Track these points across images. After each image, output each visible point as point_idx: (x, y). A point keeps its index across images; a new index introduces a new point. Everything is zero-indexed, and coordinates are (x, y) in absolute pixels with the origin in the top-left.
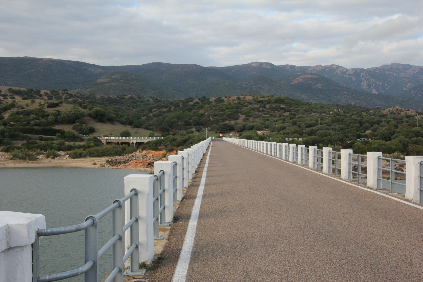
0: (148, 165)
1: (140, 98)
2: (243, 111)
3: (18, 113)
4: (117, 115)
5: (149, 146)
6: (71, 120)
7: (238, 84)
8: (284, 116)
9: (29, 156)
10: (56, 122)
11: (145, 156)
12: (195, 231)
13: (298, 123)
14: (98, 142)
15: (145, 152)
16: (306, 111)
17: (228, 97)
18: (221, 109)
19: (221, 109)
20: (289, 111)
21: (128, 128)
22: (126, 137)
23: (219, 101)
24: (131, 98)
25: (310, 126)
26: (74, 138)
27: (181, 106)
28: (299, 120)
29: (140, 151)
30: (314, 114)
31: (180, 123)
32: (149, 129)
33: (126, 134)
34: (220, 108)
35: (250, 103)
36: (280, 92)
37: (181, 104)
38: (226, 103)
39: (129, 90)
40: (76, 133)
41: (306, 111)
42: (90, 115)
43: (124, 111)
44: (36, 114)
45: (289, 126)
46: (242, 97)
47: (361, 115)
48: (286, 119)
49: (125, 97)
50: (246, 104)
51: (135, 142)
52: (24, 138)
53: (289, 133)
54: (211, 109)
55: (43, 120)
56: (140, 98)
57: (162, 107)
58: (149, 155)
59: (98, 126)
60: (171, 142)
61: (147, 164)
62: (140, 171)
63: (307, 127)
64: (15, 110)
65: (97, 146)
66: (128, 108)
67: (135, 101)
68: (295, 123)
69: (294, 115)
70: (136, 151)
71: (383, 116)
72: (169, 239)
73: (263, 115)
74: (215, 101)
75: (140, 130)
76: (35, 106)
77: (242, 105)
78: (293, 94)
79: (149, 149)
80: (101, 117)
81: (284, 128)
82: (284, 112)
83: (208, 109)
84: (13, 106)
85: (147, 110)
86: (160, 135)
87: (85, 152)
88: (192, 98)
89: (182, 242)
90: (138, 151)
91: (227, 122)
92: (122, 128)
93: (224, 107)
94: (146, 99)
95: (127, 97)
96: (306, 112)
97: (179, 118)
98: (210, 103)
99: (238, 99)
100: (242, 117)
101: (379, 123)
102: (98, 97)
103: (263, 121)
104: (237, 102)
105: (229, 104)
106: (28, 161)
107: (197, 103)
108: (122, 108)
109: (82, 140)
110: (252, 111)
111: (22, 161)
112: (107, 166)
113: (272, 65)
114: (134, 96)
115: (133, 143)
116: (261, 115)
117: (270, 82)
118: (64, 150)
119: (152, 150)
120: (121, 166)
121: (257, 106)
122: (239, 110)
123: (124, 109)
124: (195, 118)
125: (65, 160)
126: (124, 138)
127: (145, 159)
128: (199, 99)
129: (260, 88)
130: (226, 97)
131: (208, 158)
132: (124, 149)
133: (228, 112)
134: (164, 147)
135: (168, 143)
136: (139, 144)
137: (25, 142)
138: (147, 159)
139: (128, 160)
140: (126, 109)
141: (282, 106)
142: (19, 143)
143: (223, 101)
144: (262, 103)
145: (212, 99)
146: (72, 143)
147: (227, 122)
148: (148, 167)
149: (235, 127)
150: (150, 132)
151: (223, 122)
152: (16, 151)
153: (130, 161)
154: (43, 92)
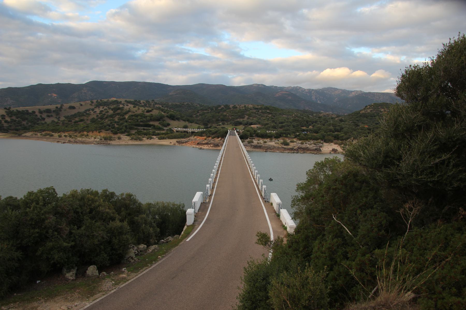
3: (132, 116)
4: (181, 116)
6: (159, 119)
9: (139, 138)
10: (151, 120)
14: (172, 131)
15: (196, 137)
16: (280, 114)
20: (271, 114)
21: (187, 123)
23: (235, 107)
24: (188, 104)
25: (282, 123)
26: (160, 129)
30: (284, 116)
33: (186, 127)
35: (251, 109)
38: (238, 109)
40: (161, 126)
41: (280, 114)
42: (167, 116)
44: (141, 116)
46: (247, 105)
47: (308, 117)
51: (190, 131)
52: (136, 129)
55: (145, 119)
57: (204, 110)
59: (172, 123)
64: (130, 114)
65: (172, 133)
68: (273, 121)
71: (320, 117)
74: (233, 107)
75: (193, 125)
76: (140, 112)
80: (172, 118)
81: (267, 124)
84: (129, 111)
87: (165, 136)
91: (238, 120)
92: (183, 123)
95: (185, 104)
98: (230, 108)
99: (245, 106)
100: (247, 117)
101: (316, 122)
102: (170, 104)
106: (138, 141)
107: (223, 108)
109: (164, 130)
111: (135, 141)
112: (177, 144)
113: (264, 86)
118: (155, 135)
121: (254, 111)
124: (222, 117)
125: (155, 140)
132: (185, 135)
136: (193, 133)
137: (136, 131)
141: (268, 111)
142: (133, 132)
143: (237, 108)
146: (159, 132)
147: (238, 120)
150: (197, 125)
152: (133, 136)
154: (142, 101)
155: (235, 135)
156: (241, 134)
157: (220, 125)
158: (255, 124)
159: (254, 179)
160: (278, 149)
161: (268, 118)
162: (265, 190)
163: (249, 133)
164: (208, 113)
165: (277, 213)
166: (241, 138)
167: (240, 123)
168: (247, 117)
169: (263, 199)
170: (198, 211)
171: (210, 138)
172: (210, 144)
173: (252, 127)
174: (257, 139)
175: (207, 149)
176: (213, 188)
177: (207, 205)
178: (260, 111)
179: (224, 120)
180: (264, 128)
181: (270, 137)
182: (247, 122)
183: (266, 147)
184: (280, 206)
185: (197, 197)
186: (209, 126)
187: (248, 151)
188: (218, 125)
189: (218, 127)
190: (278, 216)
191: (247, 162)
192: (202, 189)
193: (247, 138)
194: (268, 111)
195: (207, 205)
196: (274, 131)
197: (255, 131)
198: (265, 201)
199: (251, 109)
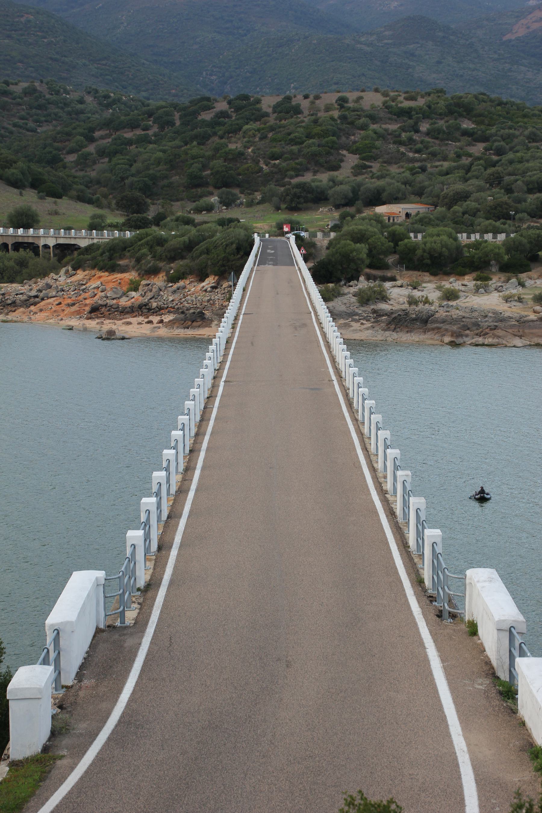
0: (91, 312)
1: (58, 93)
2: (355, 142)
5: (94, 258)
7: (347, 41)
8: (470, 155)
11: (80, 287)
12: (174, 561)
13: (507, 179)
15: (80, 275)
17: (311, 97)
18: (292, 136)
19: (292, 136)
20: (484, 139)
21: (29, 199)
22: (26, 227)
23: (287, 109)
24: (30, 92)
27: (178, 123)
28: (510, 169)
29: (67, 272)
31: (176, 178)
32: (90, 202)
34: (289, 134)
35: (373, 118)
36: (471, 66)
37: (177, 115)
38: (305, 118)
39: (21, 62)
43: (11, 133)
45: (480, 189)
46: (352, 96)
48: (474, 168)
49: (12, 88)
50: (363, 120)
51: (51, 242)
53: (478, 210)
54: (263, 138)
56: (58, 93)
58: (94, 284)
60: (151, 247)
61: (88, 309)
62: (71, 329)
63: (530, 191)
66: (21, 122)
67: (42, 101)
68: (496, 181)
69: (500, 152)
70: (56, 269)
72: (154, 569)
73: (411, 155)
74: (276, 108)
75: (65, 205)
77: (352, 123)
78: (510, 70)
79: (93, 268)
81: (464, 196)
82: (469, 145)
83: (254, 136)
85: (82, 134)
86: (121, 220)
88: (208, 99)
89: (164, 571)
90: (63, 270)
91: (307, 178)
93: (300, 132)
94: (75, 96)
96: (534, 141)
97: (174, 163)
98: (261, 116)
99: (342, 101)
100: (351, 160)
103: (407, 174)
104: (336, 114)
105: (316, 122)
107: (223, 114)
108: (5, 125)
110: (378, 143)
114: (37, 84)
115: (46, 246)
116: (403, 154)
117: (441, 34)
119: (101, 269)
120: (18, 314)
121: (393, 127)
122: (344, 139)
123: (10, 127)
124: (218, 163)
126: (21, 231)
127: (84, 295)
128: (229, 103)
129: (413, 55)
130: (306, 97)
131: (222, 384)
133: (312, 145)
134: (133, 262)
135: (145, 250)
136: (64, 250)
138: (87, 295)
139: (36, 297)
140: (15, 125)
141: (467, 125)
143: (297, 110)
144: (410, 118)
145: (268, 102)
147: (307, 178)
148: (90, 318)
149: (330, 192)
151: (297, 176)
153: (43, 299)
155: (290, 261)
156: (323, 254)
157: (209, 209)
158: (395, 199)
159: (382, 493)
160: (521, 327)
161: (466, 161)
162: (435, 555)
163: (363, 248)
164: (144, 140)
165: (504, 676)
166: (321, 275)
167: (317, 198)
168: (351, 160)
169: (428, 599)
170: (79, 676)
171: (159, 281)
172: (159, 311)
173: (378, 219)
174: (405, 277)
175: (146, 340)
176: (163, 547)
177: (129, 642)
178: (424, 127)
179: (233, 182)
180: (442, 219)
181: (477, 265)
182: (355, 191)
183: (453, 321)
184: (518, 640)
185: (76, 603)
186: (151, 214)
187: (351, 344)
188: (198, 210)
189: (198, 218)
190: (508, 693)
191: (350, 404)
192: (102, 552)
193: (355, 277)
194: (467, 125)
195: (129, 642)
196: (496, 232)
197: (396, 238)
198: (440, 615)
199: (373, 118)
